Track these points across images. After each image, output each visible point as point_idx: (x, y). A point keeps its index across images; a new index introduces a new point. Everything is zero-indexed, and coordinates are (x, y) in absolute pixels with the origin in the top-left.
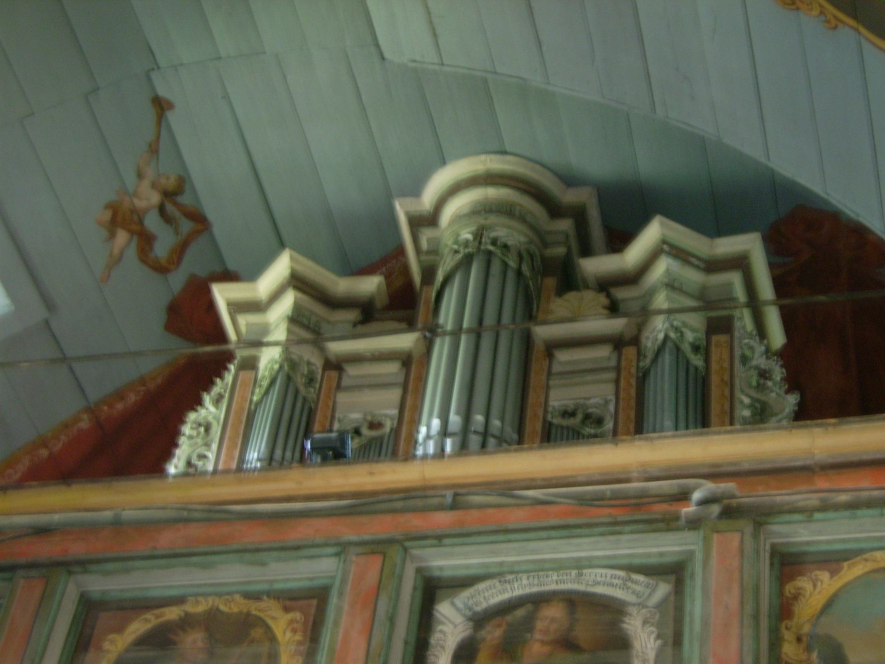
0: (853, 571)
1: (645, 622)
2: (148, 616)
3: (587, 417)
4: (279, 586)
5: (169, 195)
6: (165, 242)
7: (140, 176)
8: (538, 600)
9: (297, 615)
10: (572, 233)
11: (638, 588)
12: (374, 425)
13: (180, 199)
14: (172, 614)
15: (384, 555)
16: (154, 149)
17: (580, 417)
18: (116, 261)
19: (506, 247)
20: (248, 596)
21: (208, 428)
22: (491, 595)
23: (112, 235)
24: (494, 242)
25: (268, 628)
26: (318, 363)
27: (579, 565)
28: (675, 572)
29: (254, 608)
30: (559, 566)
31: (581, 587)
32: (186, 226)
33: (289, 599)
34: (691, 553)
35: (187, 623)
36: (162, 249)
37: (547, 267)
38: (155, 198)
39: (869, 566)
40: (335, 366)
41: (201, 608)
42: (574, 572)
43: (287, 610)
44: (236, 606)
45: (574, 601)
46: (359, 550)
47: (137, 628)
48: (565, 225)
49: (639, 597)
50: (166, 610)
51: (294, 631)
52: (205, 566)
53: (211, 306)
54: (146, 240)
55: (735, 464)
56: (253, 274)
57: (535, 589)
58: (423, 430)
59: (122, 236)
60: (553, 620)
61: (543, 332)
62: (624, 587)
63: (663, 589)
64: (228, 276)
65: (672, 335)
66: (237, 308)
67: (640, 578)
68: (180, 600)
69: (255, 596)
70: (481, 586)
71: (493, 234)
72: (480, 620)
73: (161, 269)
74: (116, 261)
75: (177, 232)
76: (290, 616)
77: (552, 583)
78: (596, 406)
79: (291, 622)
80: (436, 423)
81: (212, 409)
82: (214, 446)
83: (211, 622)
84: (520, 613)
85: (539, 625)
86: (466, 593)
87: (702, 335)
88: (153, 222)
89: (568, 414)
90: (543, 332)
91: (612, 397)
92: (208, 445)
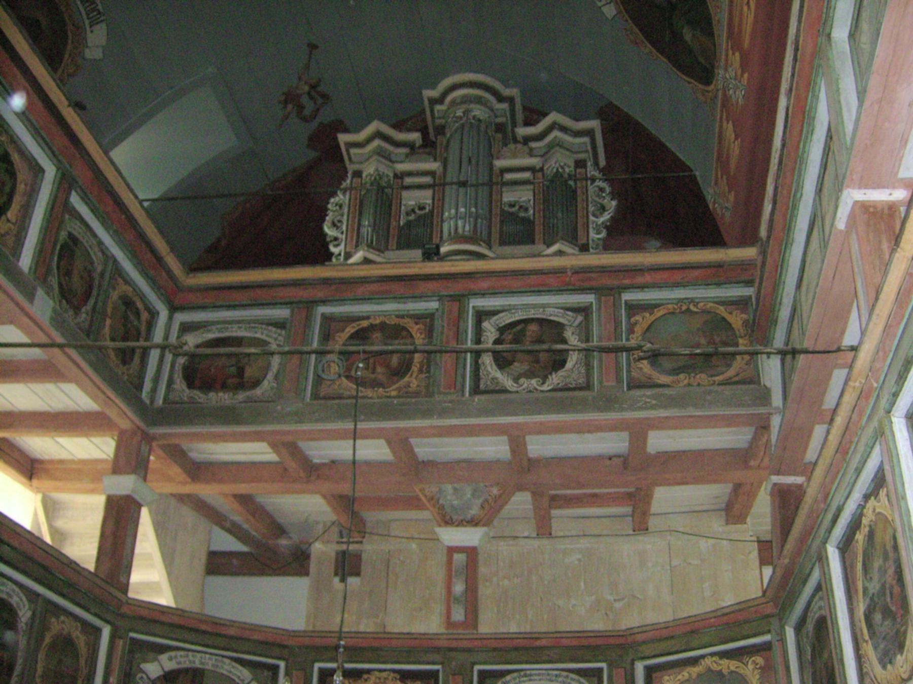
0: (659, 313)
1: (573, 333)
2: (354, 325)
3: (521, 207)
4: (411, 312)
5: (313, 87)
6: (309, 107)
7: (300, 79)
8: (526, 321)
9: (421, 326)
10: (508, 109)
11: (570, 318)
12: (422, 208)
13: (319, 89)
14: (365, 324)
15: (459, 301)
16: (307, 67)
17: (517, 207)
18: (286, 117)
19: (479, 120)
20: (398, 316)
21: (341, 206)
22: (506, 319)
23: (285, 107)
24: (474, 117)
25: (408, 331)
26: (391, 175)
27: (544, 306)
28: (584, 310)
29: (402, 322)
30: (534, 306)
31: (544, 317)
32: (320, 101)
33: (418, 318)
34: (592, 303)
35: (372, 327)
36: (307, 112)
37: (500, 128)
38: (307, 88)
39: (665, 311)
40: (400, 176)
41: (378, 322)
42: (541, 310)
43: (417, 324)
44: (394, 321)
45: (541, 322)
46: (449, 299)
47: (350, 330)
48: (504, 106)
49: (571, 322)
50: (361, 322)
51: (421, 333)
52: (378, 304)
53: (338, 146)
54: (301, 107)
55: (612, 267)
56: (358, 130)
57: (525, 317)
58: (446, 214)
59: (290, 106)
60: (533, 331)
61: (499, 164)
62: (563, 317)
63: (580, 318)
64: (346, 131)
65: (560, 170)
66: (350, 145)
67: (569, 313)
68: (368, 318)
69: (402, 317)
70: (501, 315)
71: (473, 114)
72: (502, 330)
73: (305, 120)
74: (286, 117)
75: (315, 103)
76: (418, 326)
77: (532, 314)
78: (524, 202)
79: (419, 329)
80: (453, 211)
81: (341, 196)
82: (345, 217)
83: (383, 327)
84: (519, 328)
85: (528, 334)
86: (496, 317)
87: (572, 169)
88: (305, 100)
89: (512, 205)
90: (499, 164)
91: (532, 198)
92: (342, 215)
